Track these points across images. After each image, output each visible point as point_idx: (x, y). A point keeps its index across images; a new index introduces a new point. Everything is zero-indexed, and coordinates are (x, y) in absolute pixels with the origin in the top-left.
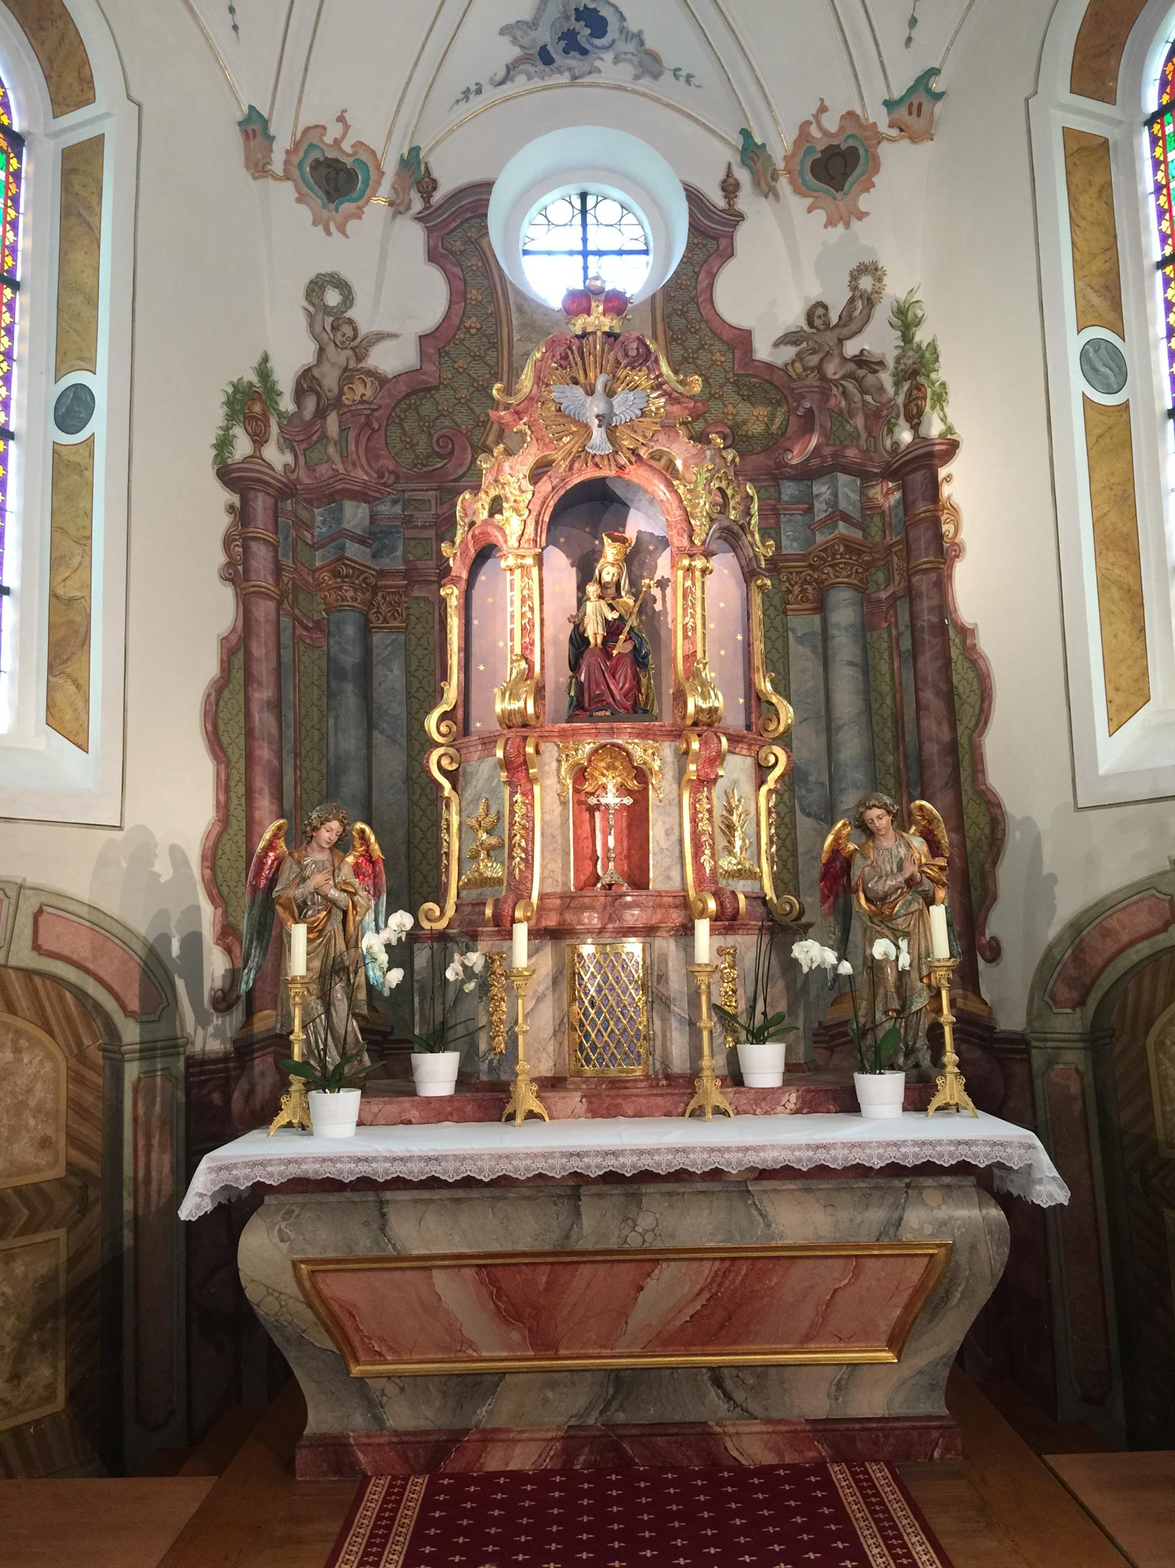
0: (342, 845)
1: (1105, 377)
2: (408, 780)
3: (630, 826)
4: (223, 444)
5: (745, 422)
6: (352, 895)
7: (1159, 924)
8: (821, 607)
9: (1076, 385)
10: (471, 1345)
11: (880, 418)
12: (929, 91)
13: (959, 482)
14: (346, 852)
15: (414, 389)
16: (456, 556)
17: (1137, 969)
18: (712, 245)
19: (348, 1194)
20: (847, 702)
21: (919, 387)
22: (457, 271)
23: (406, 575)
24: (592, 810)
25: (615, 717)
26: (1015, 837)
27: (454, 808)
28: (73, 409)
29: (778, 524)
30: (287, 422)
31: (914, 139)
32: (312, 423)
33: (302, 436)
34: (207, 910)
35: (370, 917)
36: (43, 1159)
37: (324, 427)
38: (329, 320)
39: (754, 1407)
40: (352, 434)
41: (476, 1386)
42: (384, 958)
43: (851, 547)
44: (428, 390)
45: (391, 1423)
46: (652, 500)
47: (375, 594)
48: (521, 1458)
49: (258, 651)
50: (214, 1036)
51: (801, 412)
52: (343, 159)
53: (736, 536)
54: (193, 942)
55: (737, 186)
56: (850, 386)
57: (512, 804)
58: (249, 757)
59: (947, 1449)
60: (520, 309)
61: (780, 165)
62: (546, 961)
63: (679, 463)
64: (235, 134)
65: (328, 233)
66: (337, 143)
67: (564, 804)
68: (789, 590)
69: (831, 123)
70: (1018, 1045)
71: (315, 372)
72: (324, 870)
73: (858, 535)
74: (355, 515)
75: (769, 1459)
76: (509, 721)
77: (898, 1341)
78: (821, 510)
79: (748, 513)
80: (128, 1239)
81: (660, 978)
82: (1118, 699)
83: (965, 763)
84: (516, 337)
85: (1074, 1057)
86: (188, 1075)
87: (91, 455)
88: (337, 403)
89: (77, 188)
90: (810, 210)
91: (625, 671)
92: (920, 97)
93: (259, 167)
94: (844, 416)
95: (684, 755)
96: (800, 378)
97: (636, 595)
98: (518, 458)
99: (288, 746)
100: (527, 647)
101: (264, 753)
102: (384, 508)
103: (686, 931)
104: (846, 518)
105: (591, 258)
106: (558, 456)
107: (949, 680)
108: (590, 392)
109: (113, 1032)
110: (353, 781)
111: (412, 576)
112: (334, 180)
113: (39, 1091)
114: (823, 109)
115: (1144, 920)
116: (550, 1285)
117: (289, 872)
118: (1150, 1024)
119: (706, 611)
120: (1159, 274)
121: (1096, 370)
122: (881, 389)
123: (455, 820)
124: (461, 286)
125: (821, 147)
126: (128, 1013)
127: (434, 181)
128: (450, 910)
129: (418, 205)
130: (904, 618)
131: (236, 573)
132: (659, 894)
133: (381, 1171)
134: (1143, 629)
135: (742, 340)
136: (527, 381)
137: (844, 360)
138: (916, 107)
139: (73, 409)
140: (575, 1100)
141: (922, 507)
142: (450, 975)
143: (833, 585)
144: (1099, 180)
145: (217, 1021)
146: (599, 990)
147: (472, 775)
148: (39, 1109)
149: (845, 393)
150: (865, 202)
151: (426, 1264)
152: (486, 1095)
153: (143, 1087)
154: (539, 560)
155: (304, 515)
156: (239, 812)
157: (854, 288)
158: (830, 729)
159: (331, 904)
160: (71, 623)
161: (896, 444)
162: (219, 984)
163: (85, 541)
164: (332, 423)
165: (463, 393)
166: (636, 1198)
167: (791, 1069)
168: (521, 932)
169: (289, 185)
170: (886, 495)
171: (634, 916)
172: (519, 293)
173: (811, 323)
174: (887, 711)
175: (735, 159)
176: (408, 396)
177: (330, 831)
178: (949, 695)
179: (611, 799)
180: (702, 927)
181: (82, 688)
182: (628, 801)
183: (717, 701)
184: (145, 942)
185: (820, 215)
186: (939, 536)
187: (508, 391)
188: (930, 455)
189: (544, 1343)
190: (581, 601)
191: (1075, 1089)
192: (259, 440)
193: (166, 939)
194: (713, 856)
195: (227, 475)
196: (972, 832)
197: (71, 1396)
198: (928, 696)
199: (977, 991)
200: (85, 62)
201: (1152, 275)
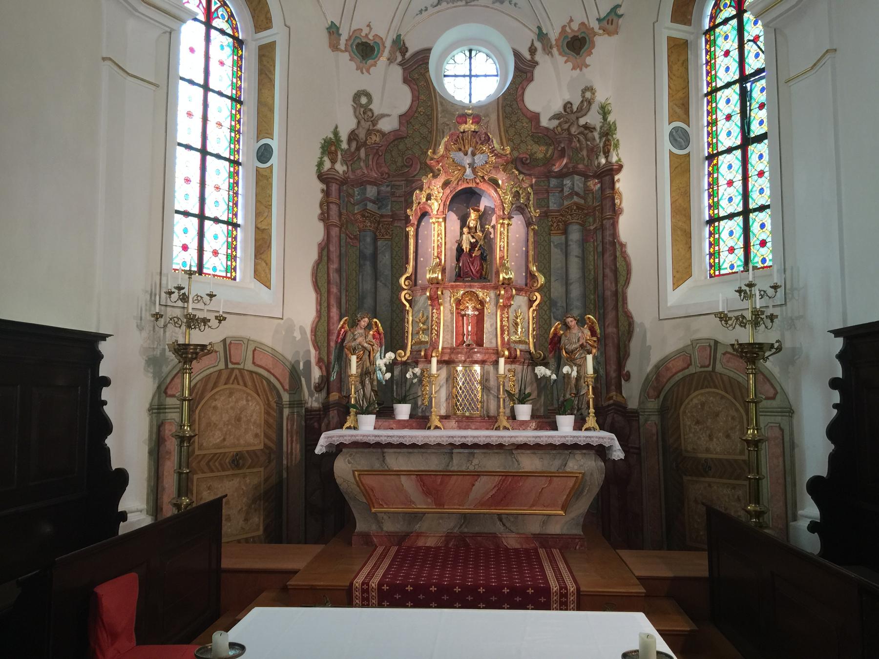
0: (369, 327)
1: (680, 143)
2: (392, 302)
3: (477, 323)
4: (320, 164)
5: (535, 153)
6: (372, 346)
7: (686, 366)
8: (565, 232)
9: (667, 146)
10: (414, 503)
11: (593, 152)
12: (616, 14)
13: (623, 183)
14: (370, 330)
15: (397, 137)
16: (412, 214)
17: (677, 384)
18: (524, 76)
19: (371, 449)
20: (575, 272)
21: (608, 140)
22: (416, 87)
23: (392, 216)
24: (463, 316)
25: (473, 280)
26: (637, 330)
27: (410, 314)
28: (264, 154)
29: (548, 196)
30: (344, 152)
31: (610, 34)
32: (355, 152)
33: (350, 158)
34: (313, 351)
35: (378, 354)
36: (256, 441)
37: (359, 154)
38: (362, 110)
39: (513, 528)
40: (371, 157)
41: (416, 517)
42: (384, 369)
43: (579, 207)
44: (402, 138)
45: (385, 529)
46: (490, 196)
47: (379, 224)
48: (431, 542)
49: (332, 248)
50: (316, 401)
51: (559, 149)
52: (369, 42)
53: (523, 209)
54: (308, 364)
55: (536, 49)
56: (581, 138)
57: (432, 313)
58: (329, 292)
59: (581, 546)
60: (442, 104)
61: (554, 43)
62: (444, 373)
63: (500, 182)
64: (325, 34)
65: (363, 73)
66: (367, 35)
67: (452, 314)
68: (546, 228)
69: (575, 26)
70: (635, 414)
71: (356, 132)
72: (363, 335)
73: (582, 202)
74: (371, 191)
75: (518, 546)
76: (432, 281)
77: (564, 508)
78: (567, 191)
79: (528, 199)
80: (285, 475)
81: (486, 380)
82: (678, 276)
83: (620, 299)
84: (440, 116)
85: (655, 418)
86: (306, 415)
87: (272, 172)
88: (365, 144)
89: (265, 63)
90: (566, 62)
91: (477, 263)
92: (613, 16)
93: (334, 47)
94: (578, 151)
95: (498, 296)
96: (560, 134)
97: (483, 232)
98: (438, 179)
99: (343, 287)
100: (439, 253)
101: (334, 290)
102: (383, 188)
103: (496, 363)
104: (577, 194)
105: (473, 78)
106: (453, 179)
107: (616, 265)
108: (466, 154)
109: (280, 397)
110: (369, 302)
111: (394, 217)
112: (365, 50)
113: (255, 416)
114: (571, 20)
115: (680, 364)
116: (442, 483)
117: (349, 337)
118: (681, 404)
119: (510, 238)
120: (705, 99)
121: (676, 140)
122: (594, 139)
123: (411, 319)
124: (417, 93)
125: (570, 36)
126: (285, 390)
127: (407, 48)
128: (408, 354)
129: (399, 58)
130: (600, 238)
131: (324, 217)
132: (487, 349)
133: (384, 440)
134: (690, 247)
135: (535, 117)
136: (441, 149)
137: (579, 126)
138: (611, 21)
139: (264, 154)
140: (453, 423)
141: (608, 192)
142: (408, 376)
143: (571, 223)
144: (682, 58)
145: (316, 395)
146: (463, 384)
147: (418, 301)
148: (255, 423)
149: (579, 141)
150: (588, 60)
151: (398, 473)
152: (420, 419)
153: (290, 418)
154: (445, 219)
155: (350, 191)
156: (325, 314)
157: (583, 97)
158: (567, 284)
159: (364, 348)
160: (263, 239)
161: (599, 163)
162: (317, 381)
163: (269, 207)
164: (363, 152)
165: (417, 140)
166: (473, 454)
167: (533, 416)
168: (434, 361)
169: (347, 54)
170: (595, 185)
171: (478, 357)
172: (441, 97)
173: (565, 111)
174: (591, 277)
175: (535, 37)
176: (394, 141)
177: (364, 322)
178: (615, 271)
179: (470, 312)
180: (502, 361)
181: (268, 264)
182: (477, 313)
183: (511, 275)
184: (291, 363)
185: (570, 65)
186: (614, 204)
187: (434, 153)
188: (612, 170)
189: (439, 504)
190: (462, 234)
191: (654, 431)
192: (333, 161)
193: (298, 362)
194: (508, 335)
195: (321, 177)
196: (622, 328)
197: (265, 530)
198: (607, 271)
199: (621, 393)
200: (268, 11)
201: (703, 100)
